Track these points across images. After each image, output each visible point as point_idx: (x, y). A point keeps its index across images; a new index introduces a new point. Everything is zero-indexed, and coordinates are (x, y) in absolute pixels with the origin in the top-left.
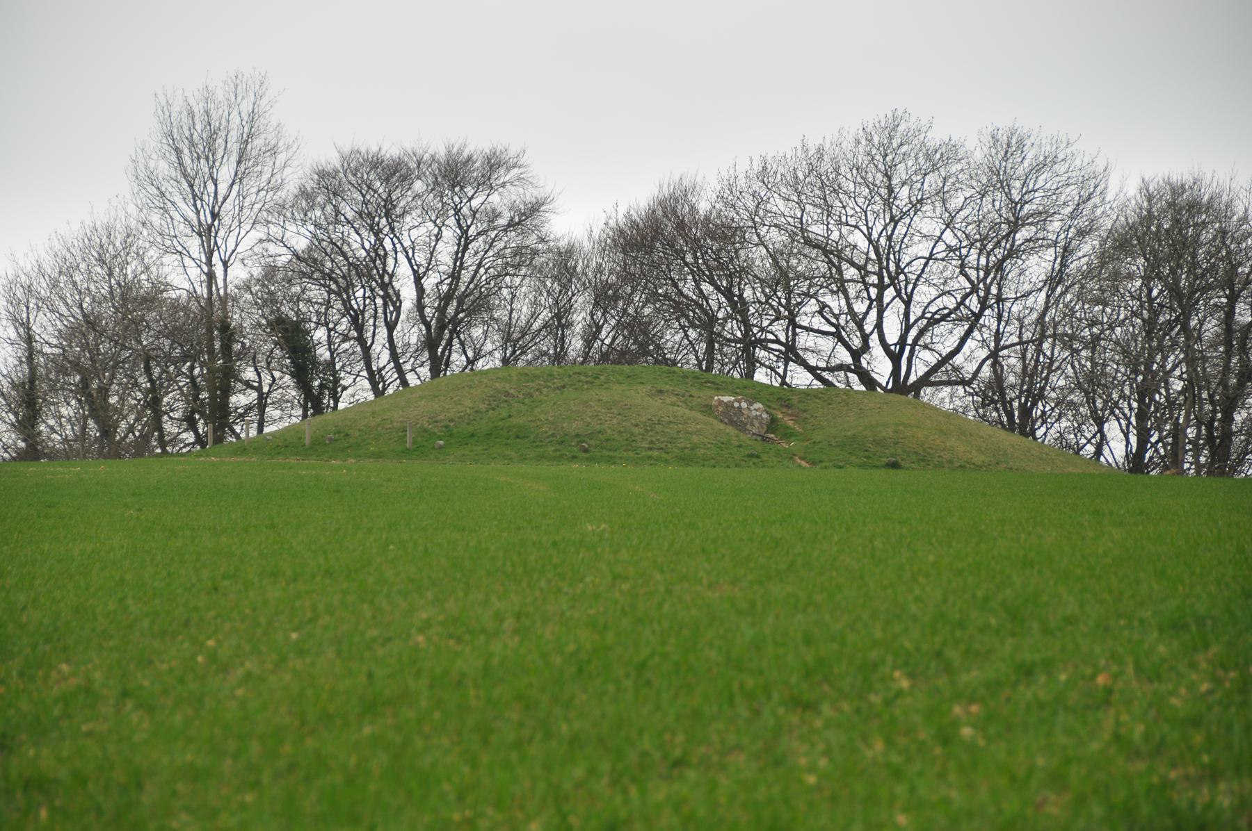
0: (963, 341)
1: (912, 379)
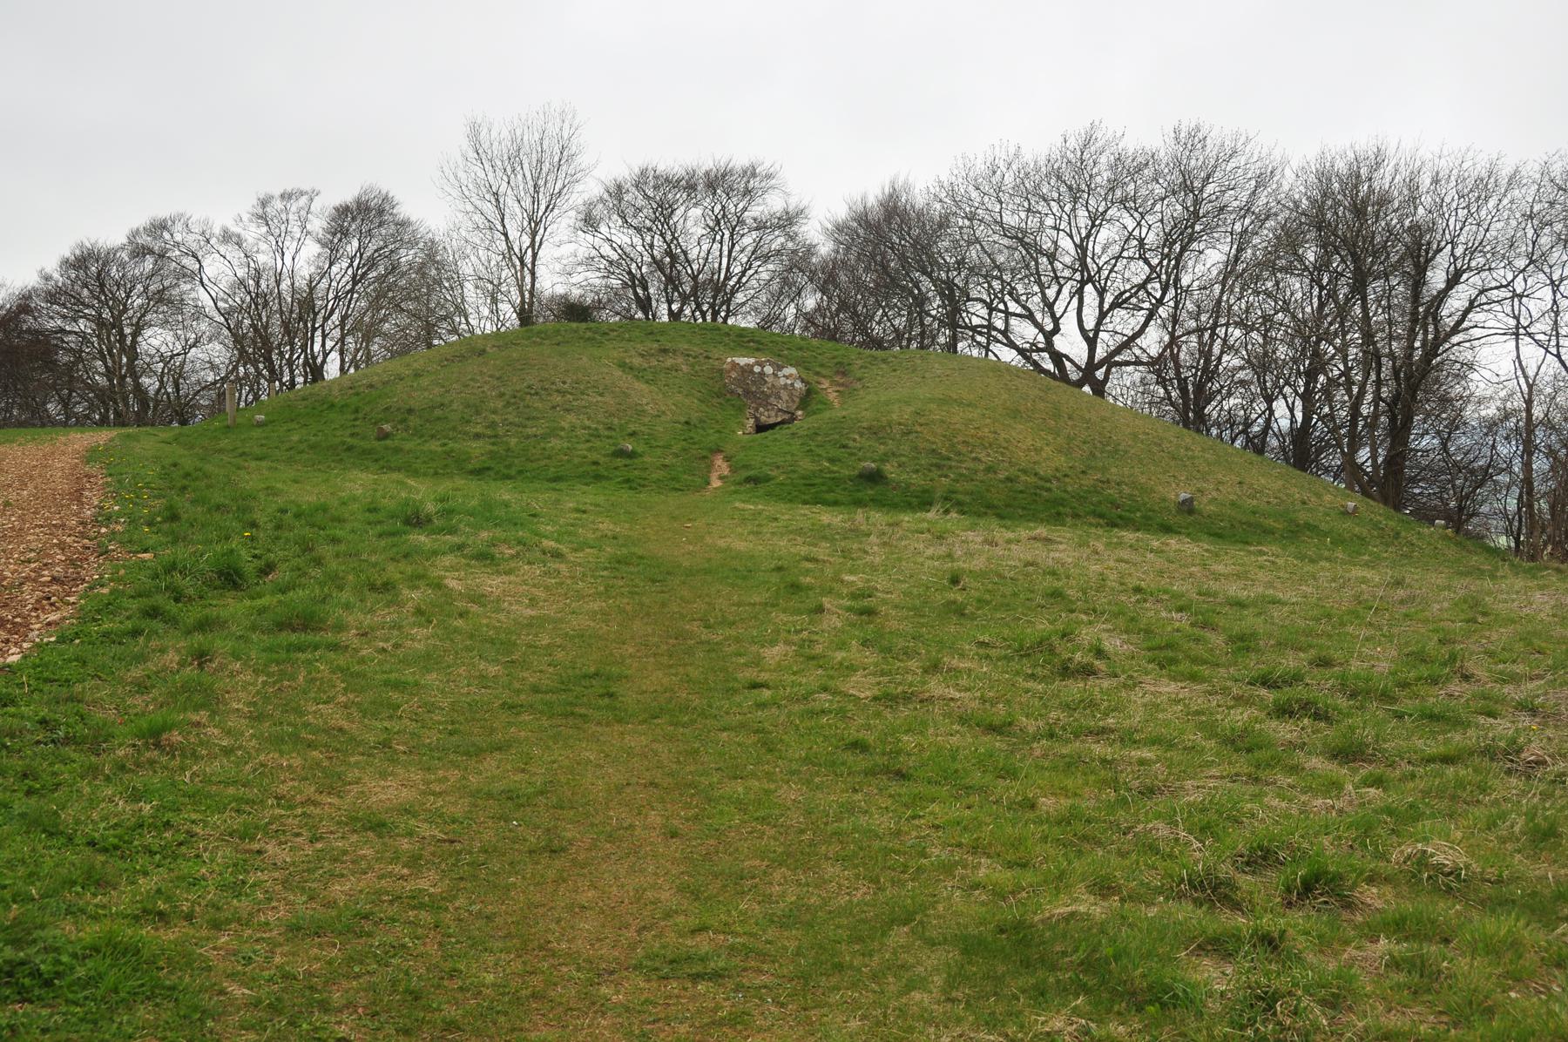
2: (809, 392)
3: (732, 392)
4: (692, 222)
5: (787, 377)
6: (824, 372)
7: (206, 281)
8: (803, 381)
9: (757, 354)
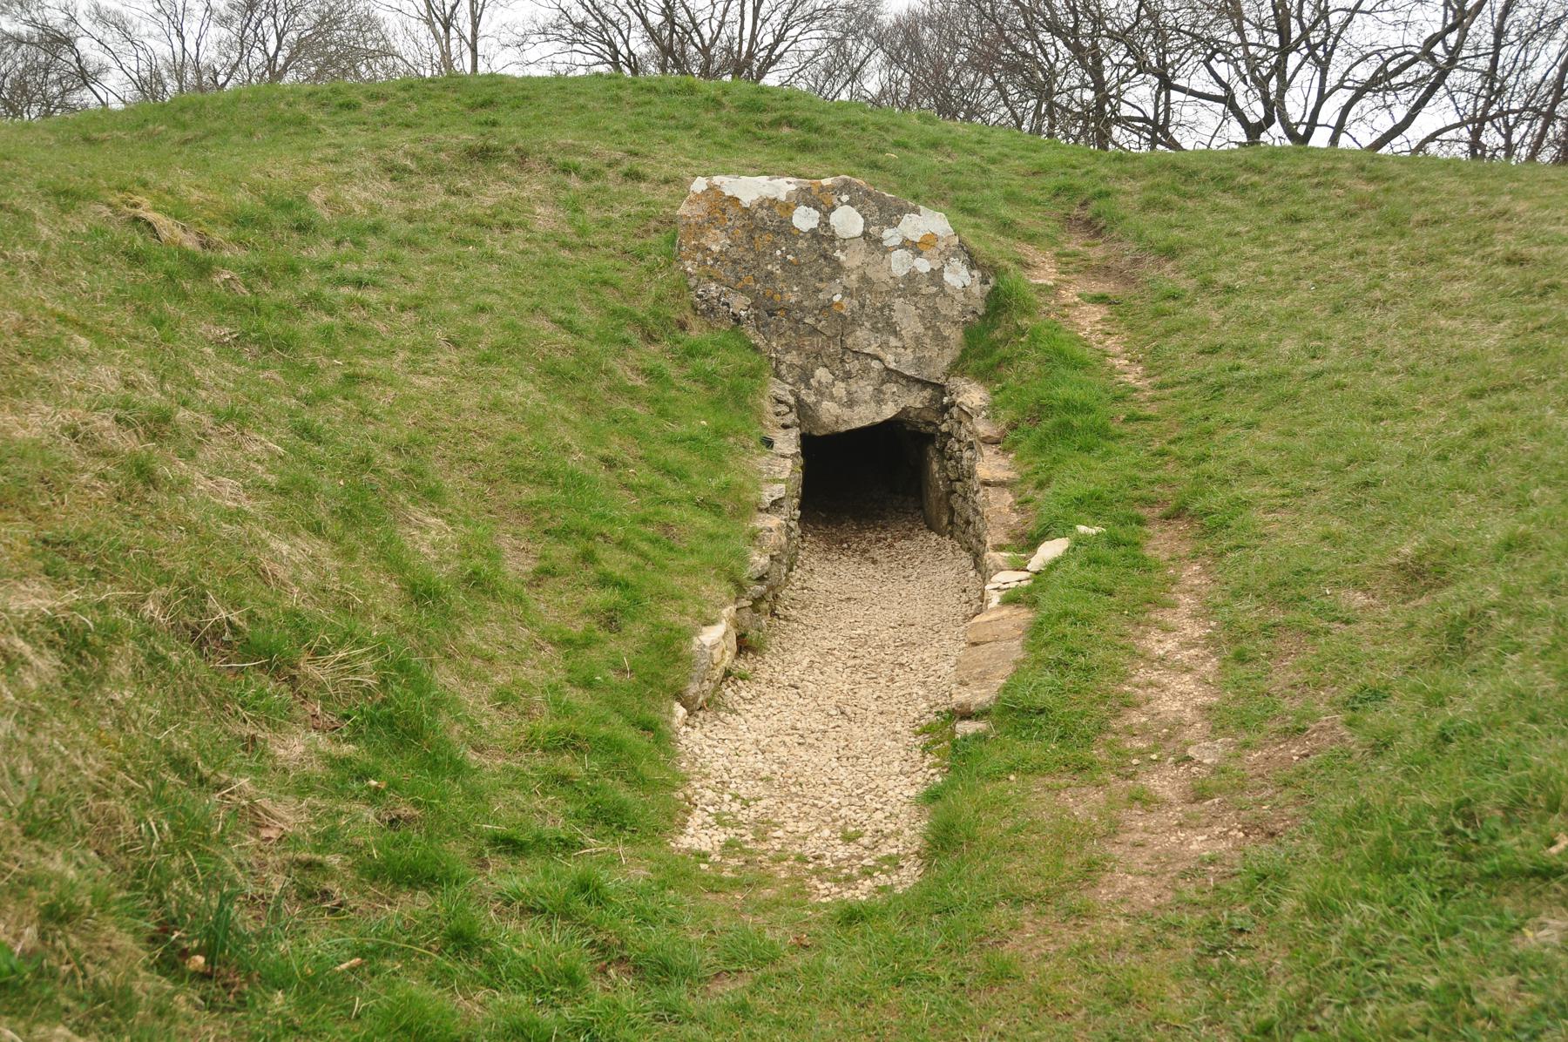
2: (999, 304)
3: (708, 311)
6: (1026, 219)
8: (973, 263)
9: (804, 161)
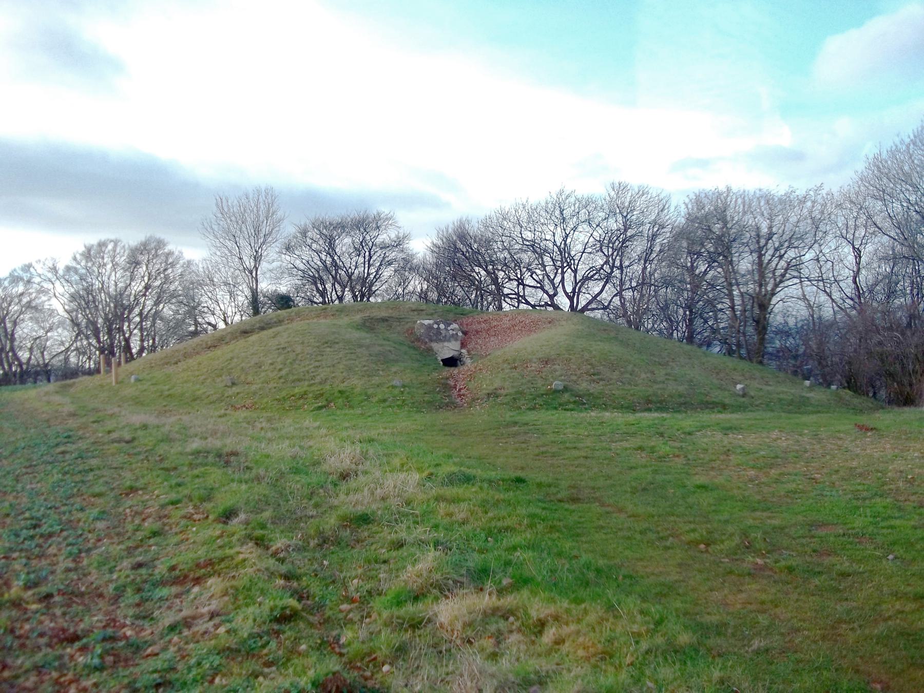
0: (604, 287)
1: (579, 307)
4: (344, 244)
5: (453, 330)
7: (57, 294)
